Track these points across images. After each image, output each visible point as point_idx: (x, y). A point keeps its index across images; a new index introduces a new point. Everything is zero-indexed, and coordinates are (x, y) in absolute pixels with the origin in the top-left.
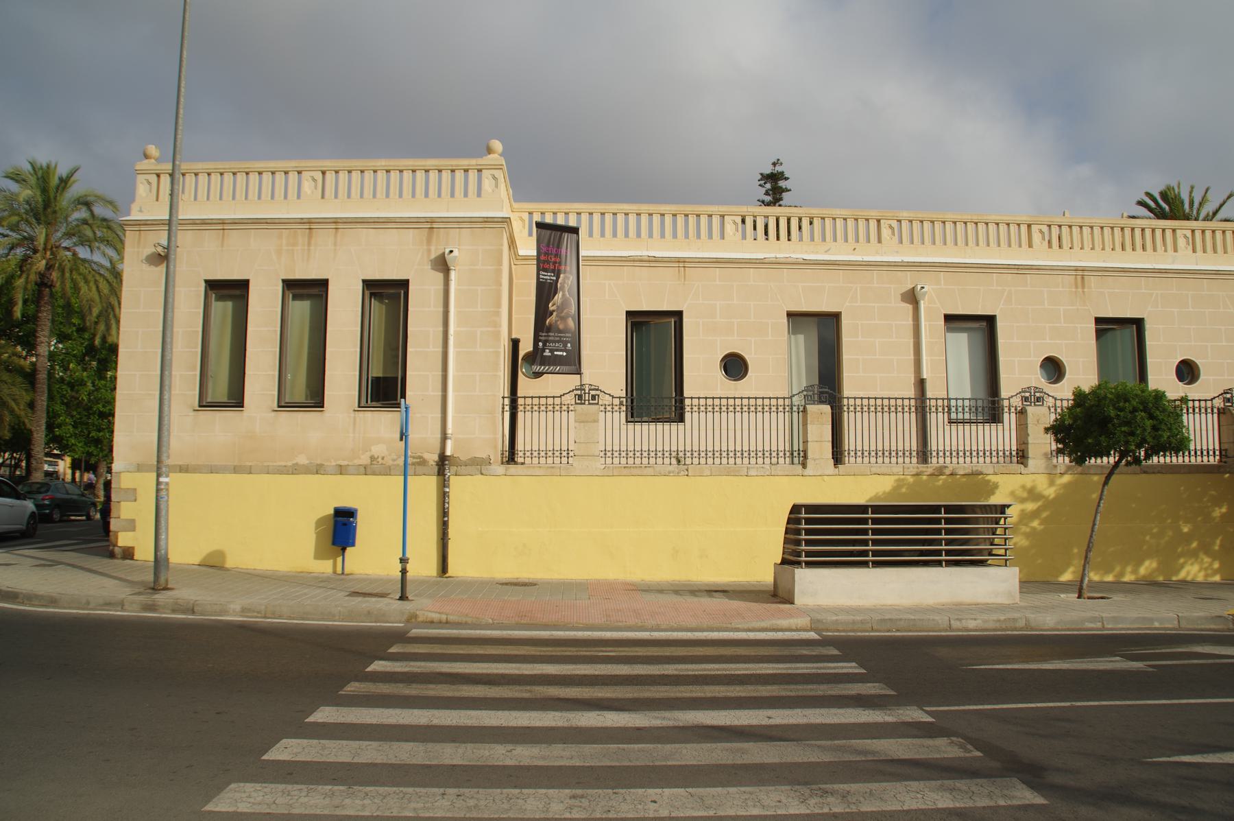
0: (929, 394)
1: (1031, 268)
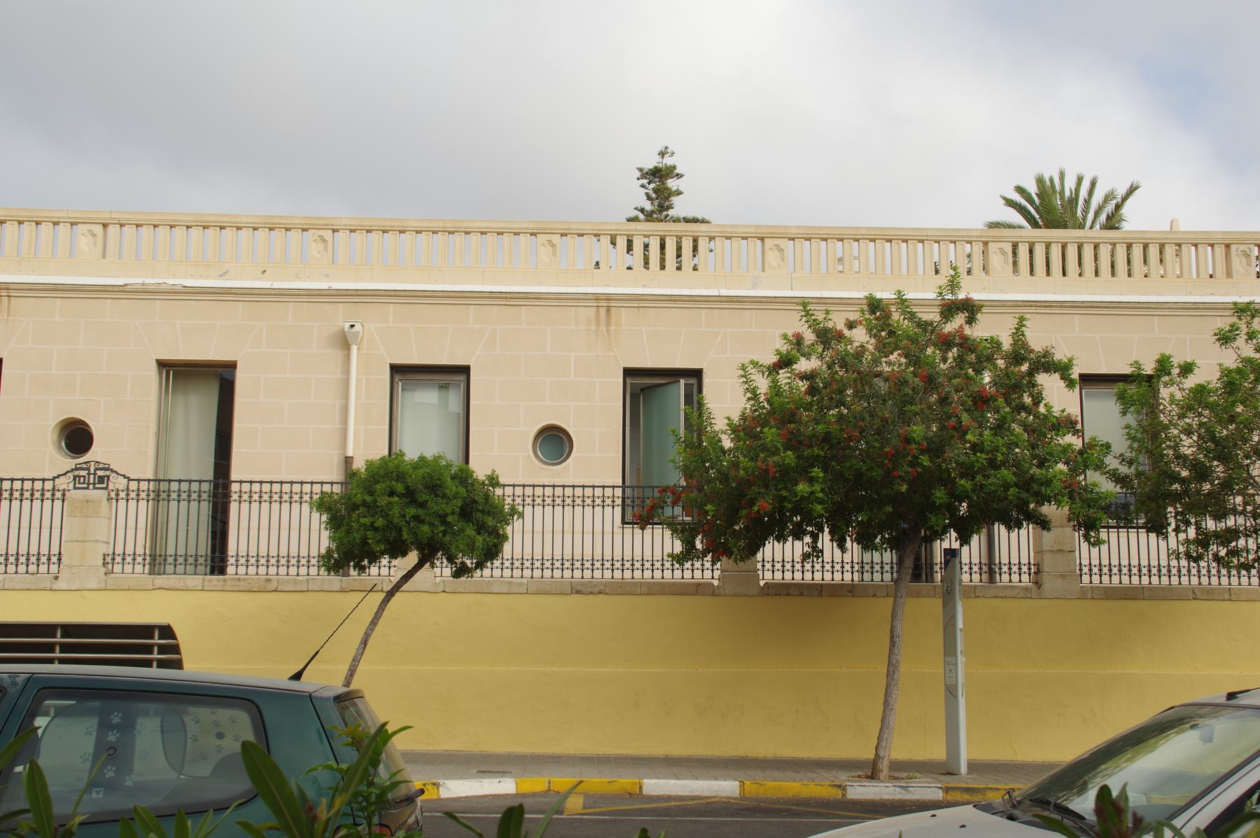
0: (234, 476)
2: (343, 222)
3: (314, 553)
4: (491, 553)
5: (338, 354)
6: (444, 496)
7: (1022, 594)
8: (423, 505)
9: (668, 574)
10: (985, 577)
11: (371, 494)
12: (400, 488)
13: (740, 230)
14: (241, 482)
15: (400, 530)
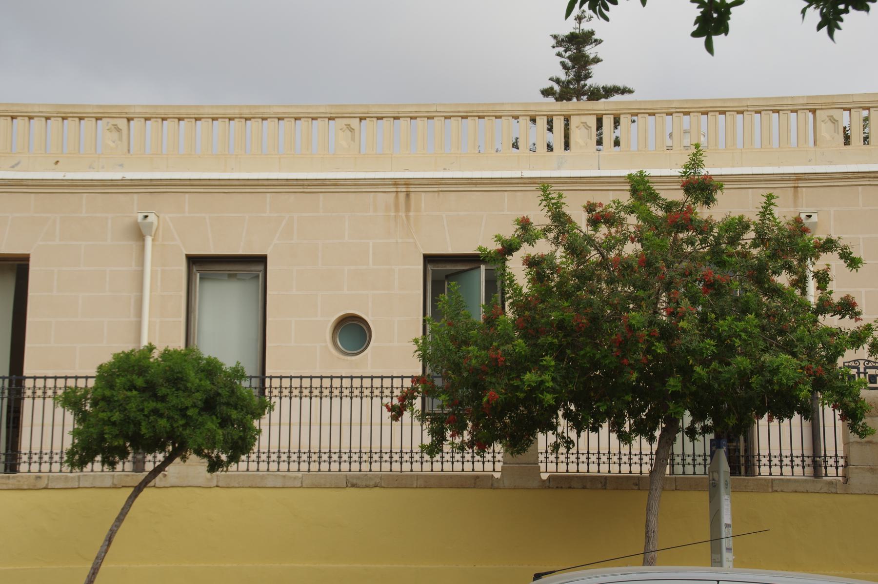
0: (27, 372)
1: (322, 183)
2: (138, 110)
3: (57, 449)
4: (240, 446)
5: (134, 245)
6: (186, 389)
7: (825, 489)
8: (163, 399)
9: (417, 467)
10: (809, 470)
11: (112, 387)
12: (140, 382)
13: (544, 108)
14: (35, 378)
15: (138, 424)
